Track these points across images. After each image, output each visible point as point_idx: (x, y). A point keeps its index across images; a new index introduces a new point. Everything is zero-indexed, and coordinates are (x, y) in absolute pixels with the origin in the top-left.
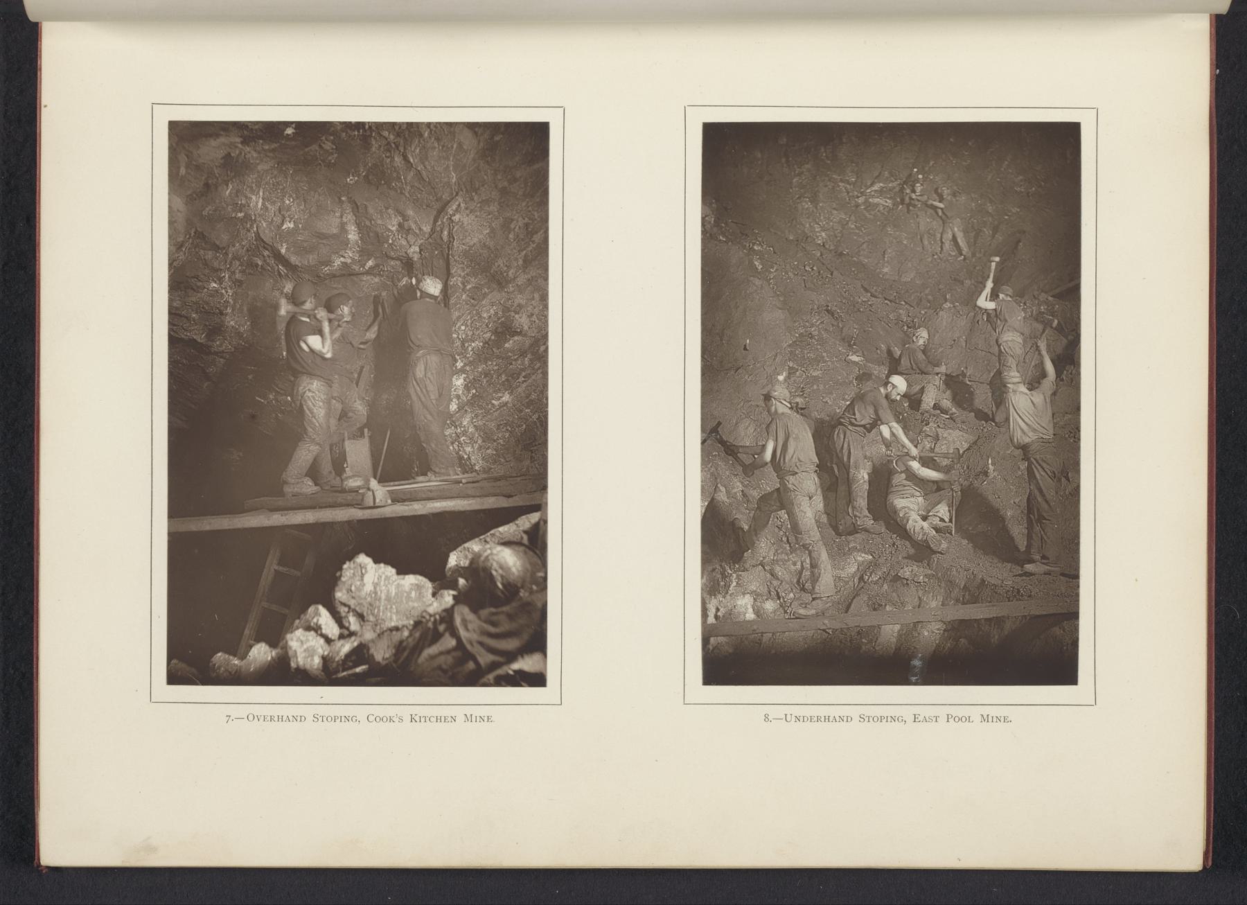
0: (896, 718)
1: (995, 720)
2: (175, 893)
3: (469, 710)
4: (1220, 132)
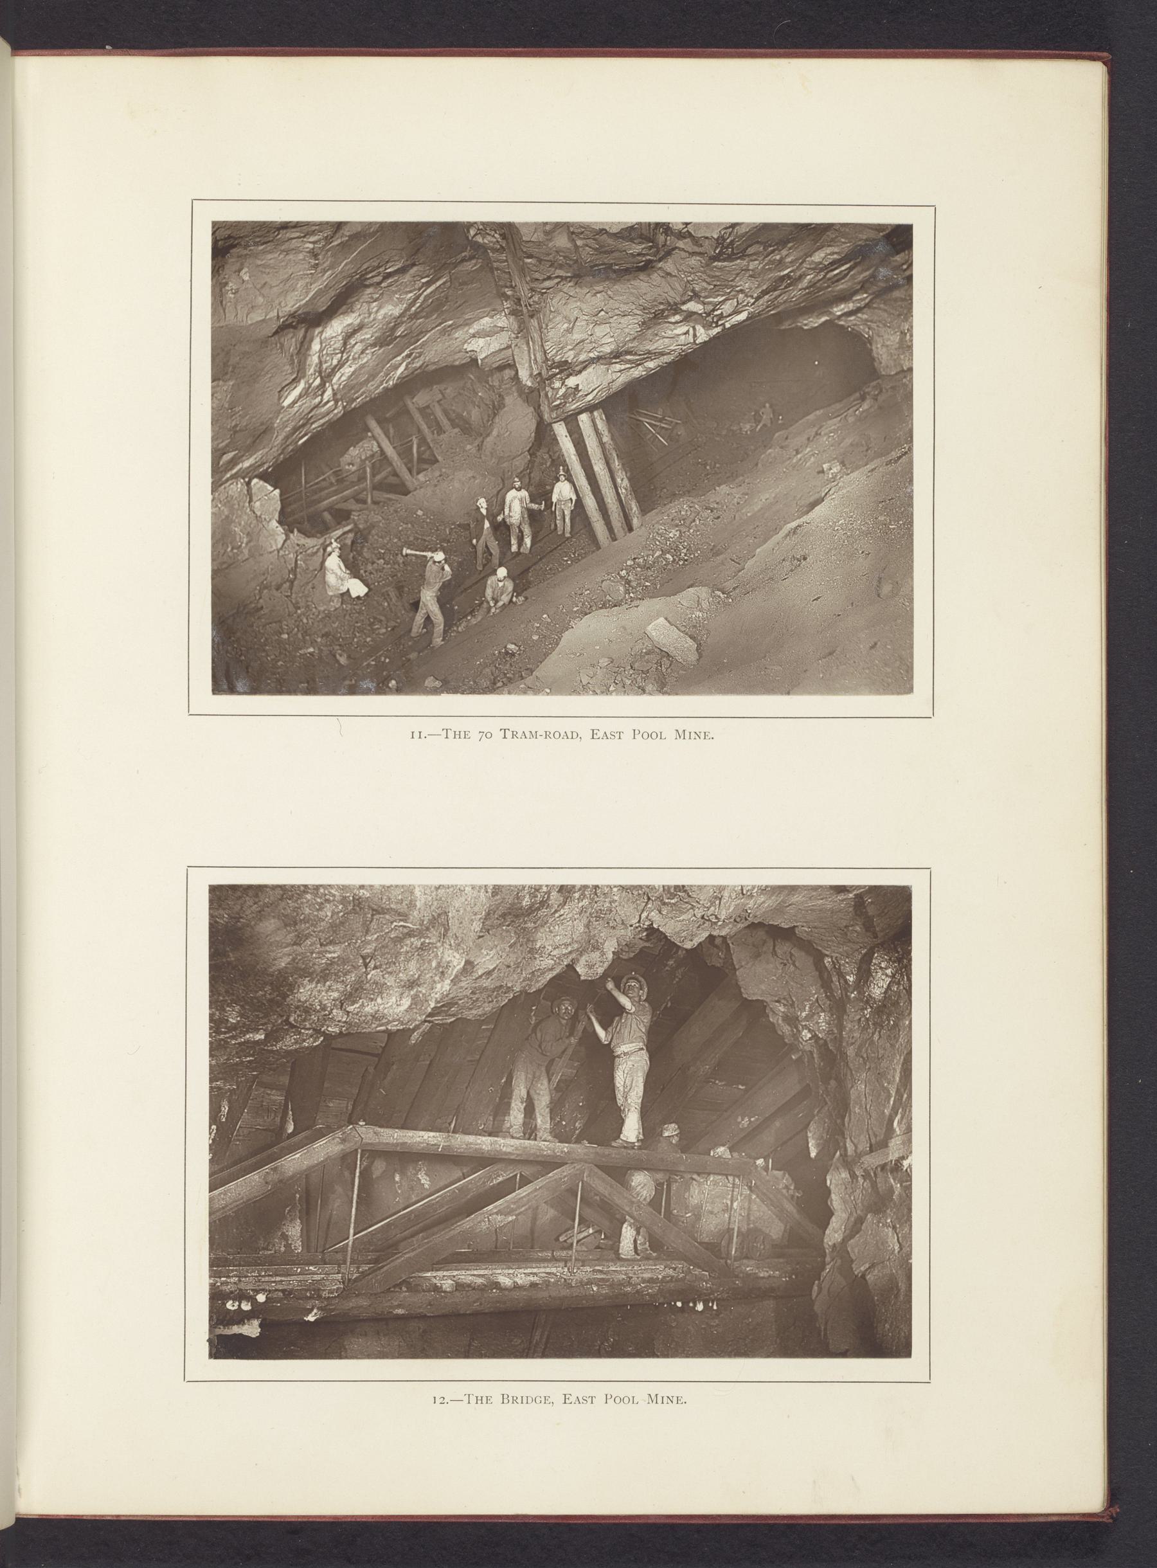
3: (681, 725)
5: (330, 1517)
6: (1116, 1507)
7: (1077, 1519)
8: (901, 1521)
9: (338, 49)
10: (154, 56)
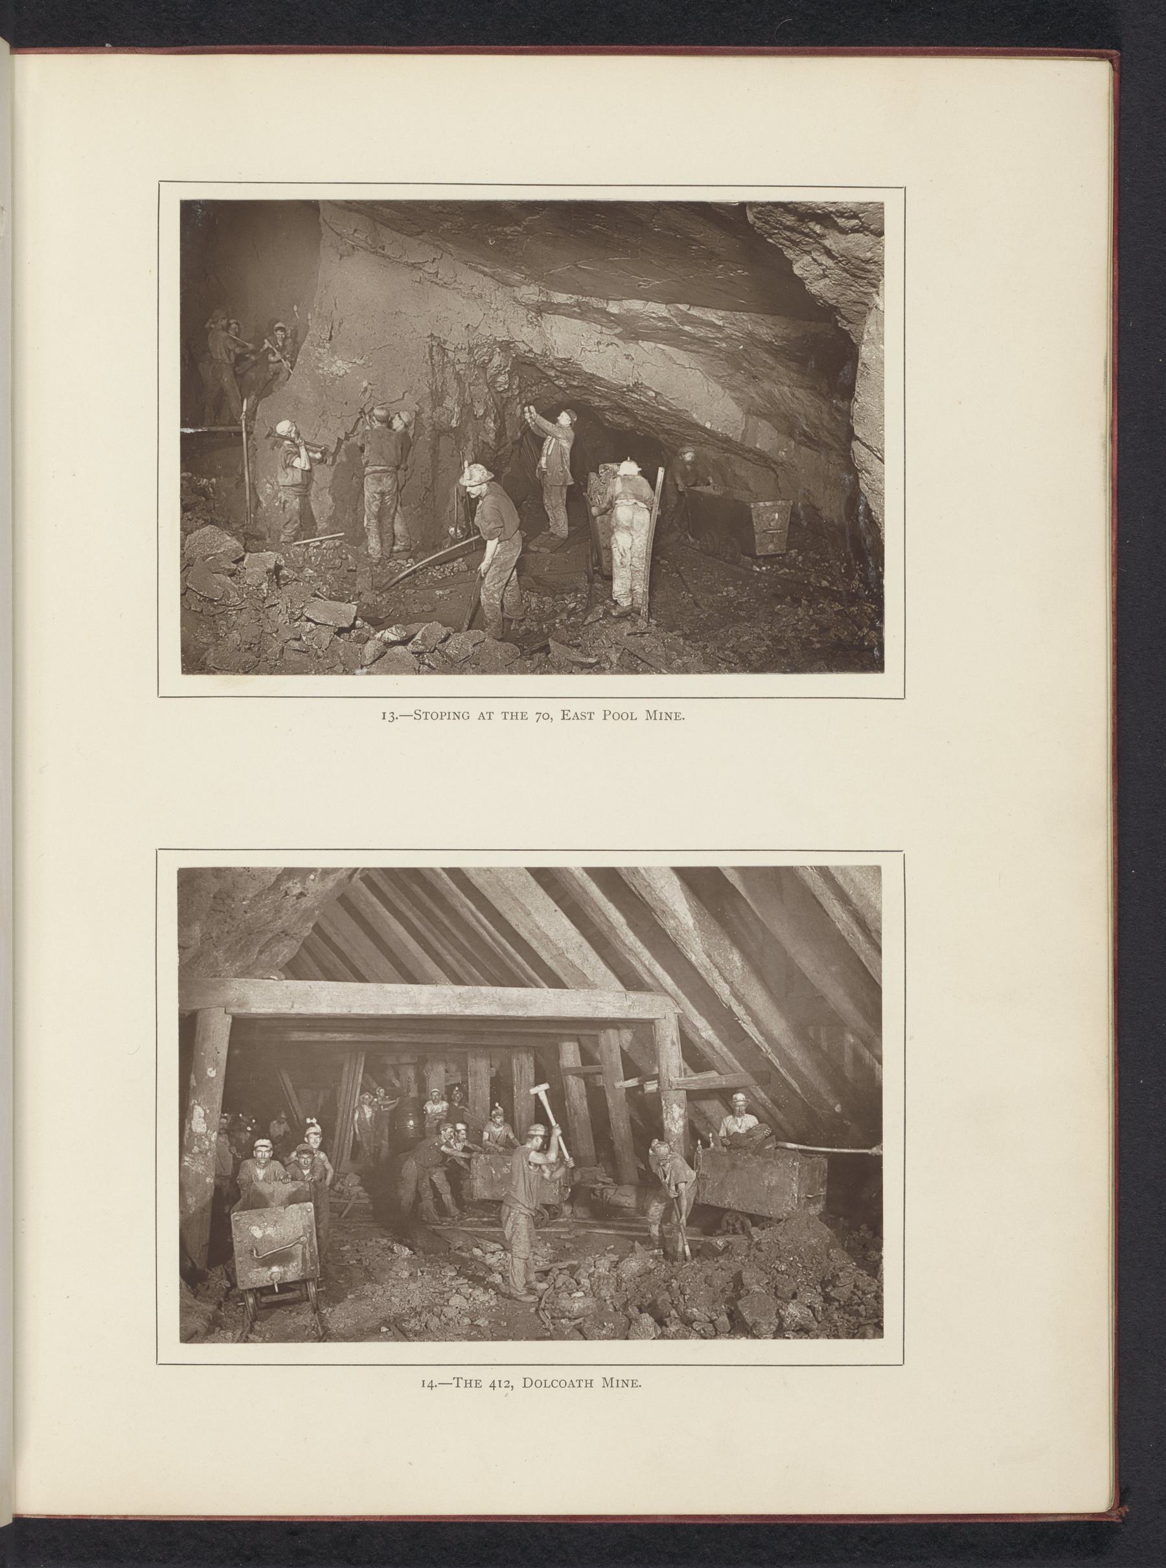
0: (461, 714)
1: (663, 717)
2: (1135, 1349)
3: (652, 705)
4: (184, 43)
5: (338, 1517)
6: (1126, 1507)
7: (1086, 1519)
8: (910, 1521)
9: (345, 47)
10: (161, 54)
